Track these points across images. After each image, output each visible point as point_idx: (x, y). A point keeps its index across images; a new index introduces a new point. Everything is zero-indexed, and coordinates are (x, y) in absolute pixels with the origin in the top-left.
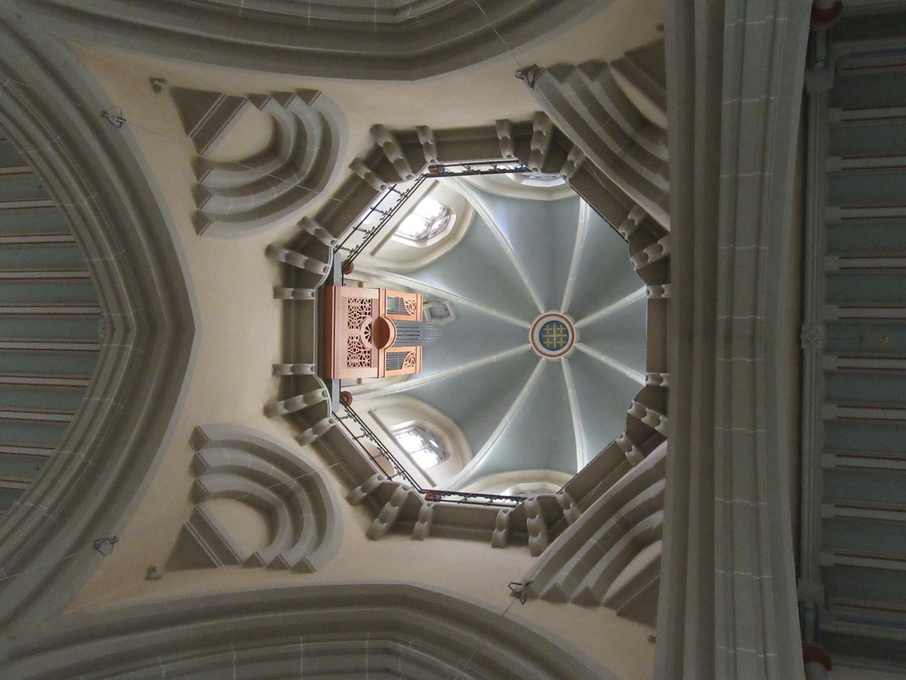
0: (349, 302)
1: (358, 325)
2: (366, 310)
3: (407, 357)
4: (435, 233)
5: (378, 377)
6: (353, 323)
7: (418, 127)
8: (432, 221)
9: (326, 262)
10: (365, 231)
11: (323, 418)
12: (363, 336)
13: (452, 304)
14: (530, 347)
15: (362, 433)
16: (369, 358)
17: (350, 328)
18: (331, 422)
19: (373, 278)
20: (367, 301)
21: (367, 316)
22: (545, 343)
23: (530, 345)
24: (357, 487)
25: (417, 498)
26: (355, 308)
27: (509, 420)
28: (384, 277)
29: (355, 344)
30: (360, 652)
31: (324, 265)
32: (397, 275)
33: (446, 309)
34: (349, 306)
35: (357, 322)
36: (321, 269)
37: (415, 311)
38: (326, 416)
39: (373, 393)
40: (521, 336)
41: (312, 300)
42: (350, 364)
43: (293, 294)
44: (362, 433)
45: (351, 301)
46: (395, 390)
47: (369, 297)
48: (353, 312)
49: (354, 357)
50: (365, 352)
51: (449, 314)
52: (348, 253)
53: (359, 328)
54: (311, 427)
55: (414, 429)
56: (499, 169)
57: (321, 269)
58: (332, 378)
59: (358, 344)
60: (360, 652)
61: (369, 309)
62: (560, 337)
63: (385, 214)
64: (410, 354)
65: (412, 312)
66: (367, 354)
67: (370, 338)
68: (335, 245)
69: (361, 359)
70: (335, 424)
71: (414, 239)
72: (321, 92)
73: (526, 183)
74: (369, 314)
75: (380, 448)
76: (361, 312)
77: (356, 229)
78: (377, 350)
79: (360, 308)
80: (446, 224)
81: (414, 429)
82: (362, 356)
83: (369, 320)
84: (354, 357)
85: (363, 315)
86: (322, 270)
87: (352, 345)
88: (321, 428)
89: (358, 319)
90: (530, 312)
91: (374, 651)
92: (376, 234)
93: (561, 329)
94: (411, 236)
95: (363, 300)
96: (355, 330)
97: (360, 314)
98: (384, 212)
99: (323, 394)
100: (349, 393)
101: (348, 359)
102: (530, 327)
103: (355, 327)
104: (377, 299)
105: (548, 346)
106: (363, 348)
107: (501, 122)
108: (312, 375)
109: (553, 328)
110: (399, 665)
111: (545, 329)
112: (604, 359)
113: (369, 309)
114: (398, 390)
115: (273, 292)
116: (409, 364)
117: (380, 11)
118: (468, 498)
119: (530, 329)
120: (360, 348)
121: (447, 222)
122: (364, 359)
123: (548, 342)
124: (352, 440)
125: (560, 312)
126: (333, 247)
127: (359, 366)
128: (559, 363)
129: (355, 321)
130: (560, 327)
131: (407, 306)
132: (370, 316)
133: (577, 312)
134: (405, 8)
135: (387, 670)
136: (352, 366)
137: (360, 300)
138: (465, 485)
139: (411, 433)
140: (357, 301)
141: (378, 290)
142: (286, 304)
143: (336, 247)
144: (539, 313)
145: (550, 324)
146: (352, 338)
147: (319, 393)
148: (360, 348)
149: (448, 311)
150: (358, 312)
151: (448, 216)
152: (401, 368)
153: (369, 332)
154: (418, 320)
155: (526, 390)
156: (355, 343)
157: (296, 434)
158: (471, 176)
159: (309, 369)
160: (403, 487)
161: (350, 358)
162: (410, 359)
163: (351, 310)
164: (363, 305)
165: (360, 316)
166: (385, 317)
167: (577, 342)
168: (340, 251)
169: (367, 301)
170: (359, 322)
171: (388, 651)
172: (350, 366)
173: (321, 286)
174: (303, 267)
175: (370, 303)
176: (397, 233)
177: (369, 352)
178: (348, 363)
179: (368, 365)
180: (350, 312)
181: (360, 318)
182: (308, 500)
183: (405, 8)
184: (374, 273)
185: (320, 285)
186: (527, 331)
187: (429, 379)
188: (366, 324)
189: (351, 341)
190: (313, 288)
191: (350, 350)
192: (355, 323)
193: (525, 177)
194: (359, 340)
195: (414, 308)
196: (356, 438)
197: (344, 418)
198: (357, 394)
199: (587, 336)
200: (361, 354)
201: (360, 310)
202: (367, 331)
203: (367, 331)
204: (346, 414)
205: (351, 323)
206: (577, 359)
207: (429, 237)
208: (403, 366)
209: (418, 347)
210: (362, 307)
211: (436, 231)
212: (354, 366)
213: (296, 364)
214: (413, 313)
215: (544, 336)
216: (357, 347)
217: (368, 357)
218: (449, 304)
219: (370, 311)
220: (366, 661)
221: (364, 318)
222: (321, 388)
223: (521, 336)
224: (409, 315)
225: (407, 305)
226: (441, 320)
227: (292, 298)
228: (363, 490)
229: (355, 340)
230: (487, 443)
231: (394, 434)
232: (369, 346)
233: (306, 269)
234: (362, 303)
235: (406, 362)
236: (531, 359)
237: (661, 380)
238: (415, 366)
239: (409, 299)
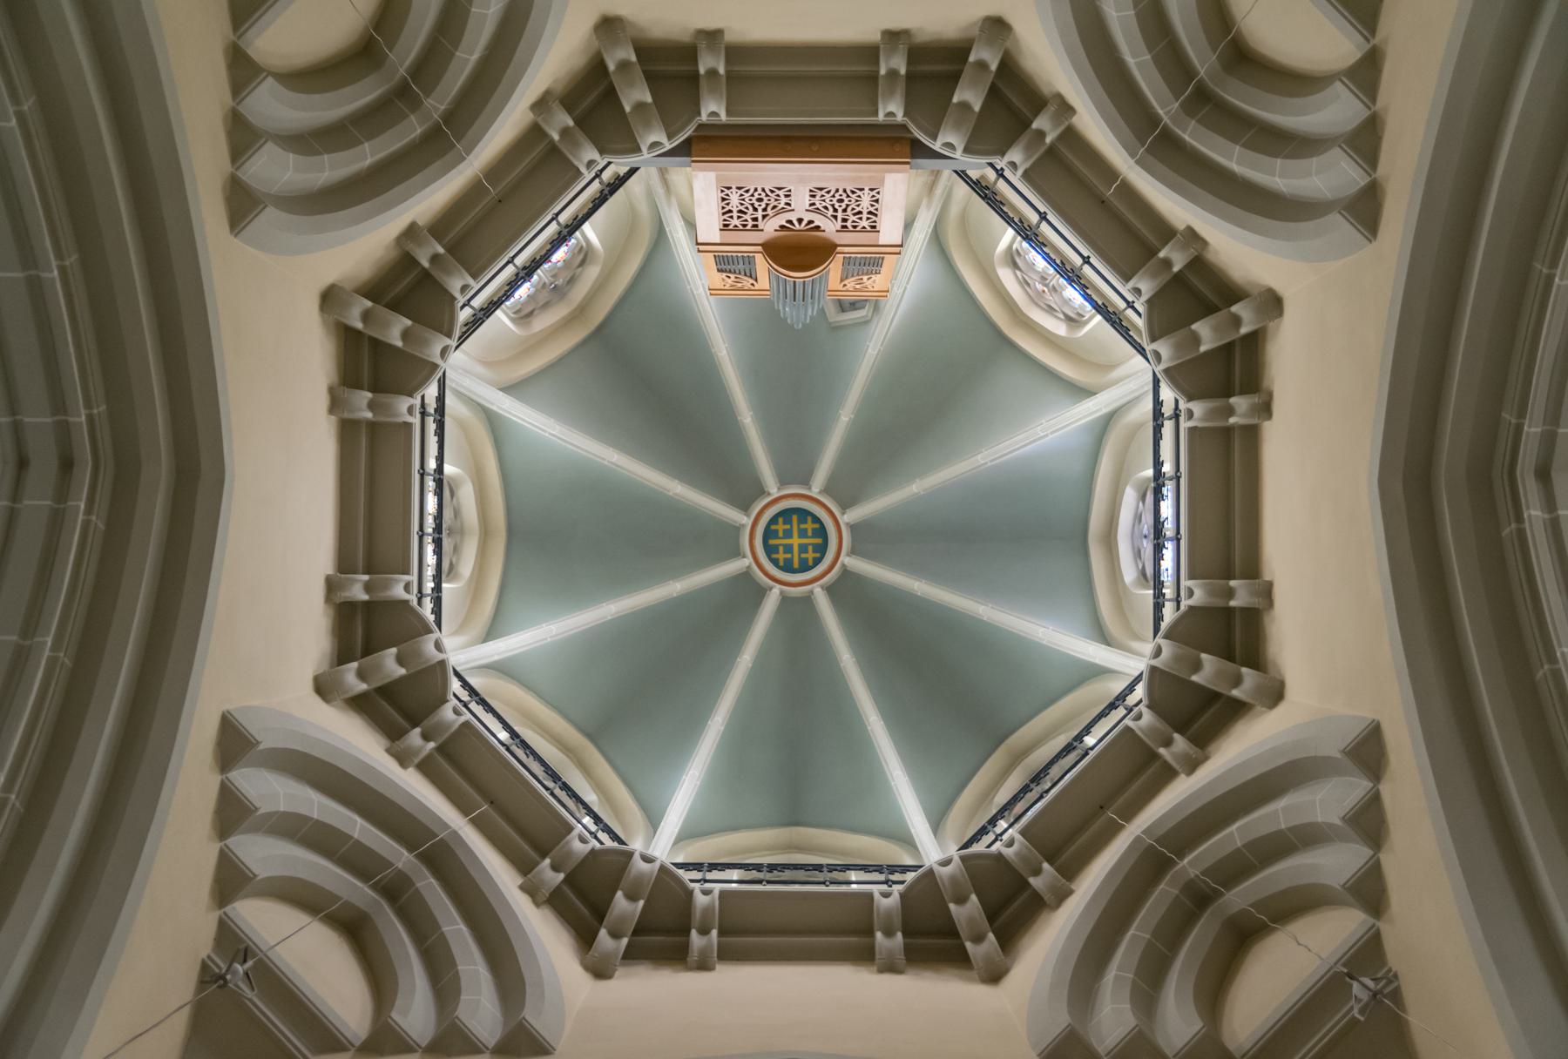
0: (872, 190)
1: (818, 206)
2: (854, 222)
4: (1025, 284)
5: (698, 244)
6: (823, 196)
7: (1270, 395)
12: (794, 217)
14: (771, 491)
16: (741, 227)
17: (811, 191)
20: (875, 222)
21: (839, 223)
23: (774, 492)
24: (440, 243)
25: (424, 382)
26: (857, 201)
28: (929, 206)
29: (773, 200)
30: (59, 404)
35: (824, 204)
36: (952, 139)
40: (795, 469)
41: (876, 113)
45: (874, 193)
49: (743, 200)
50: (755, 219)
51: (843, 310)
53: (812, 208)
54: (575, 123)
55: (582, 247)
56: (1162, 426)
57: (952, 139)
60: (59, 404)
62: (792, 552)
66: (750, 223)
72: (1370, 241)
73: (1129, 497)
74: (843, 227)
78: (760, 242)
79: (858, 209)
80: (1045, 307)
82: (745, 213)
83: (830, 228)
84: (743, 200)
85: (840, 215)
86: (950, 138)
87: (773, 195)
90: (846, 490)
91: (64, 433)
93: (810, 556)
95: (876, 215)
96: (807, 200)
97: (845, 210)
102: (815, 491)
103: (813, 200)
105: (773, 527)
106: (764, 217)
107: (1267, 592)
109: (812, 537)
110: (37, 503)
111: (809, 519)
112: (746, 659)
113: (855, 227)
115: (898, 30)
117: (1549, 441)
118: (432, 418)
120: (765, 210)
123: (781, 527)
125: (848, 555)
127: (723, 208)
128: (737, 553)
130: (814, 552)
132: (839, 228)
133: (847, 591)
134: (1550, 504)
135: (22, 463)
136: (723, 195)
137: (877, 210)
138: (459, 395)
142: (869, 53)
145: (822, 532)
146: (786, 196)
147: (658, 135)
152: (719, 270)
155: (677, 489)
158: (1152, 410)
159: (713, 108)
160: (448, 346)
161: (741, 192)
167: (782, 592)
171: (67, 465)
172: (722, 191)
173: (912, 133)
175: (869, 229)
177: (756, 226)
178: (729, 188)
179: (725, 225)
181: (836, 210)
182: (404, 142)
183: (1550, 504)
185: (913, 131)
186: (806, 482)
187: (697, 289)
188: (819, 220)
189: (781, 193)
190: (904, 116)
192: (824, 201)
193: (1142, 492)
194: (783, 208)
199: (797, 613)
201: (853, 209)
205: (823, 192)
206: (746, 593)
208: (725, 274)
210: (860, 213)
212: (723, 199)
213: (724, 80)
215: (795, 518)
217: (745, 226)
218: (867, 316)
219: (851, 229)
220: (37, 419)
221: (835, 217)
223: (795, 469)
228: (435, 258)
229: (784, 200)
232: (770, 228)
234: (870, 213)
236: (744, 491)
237: (704, 932)
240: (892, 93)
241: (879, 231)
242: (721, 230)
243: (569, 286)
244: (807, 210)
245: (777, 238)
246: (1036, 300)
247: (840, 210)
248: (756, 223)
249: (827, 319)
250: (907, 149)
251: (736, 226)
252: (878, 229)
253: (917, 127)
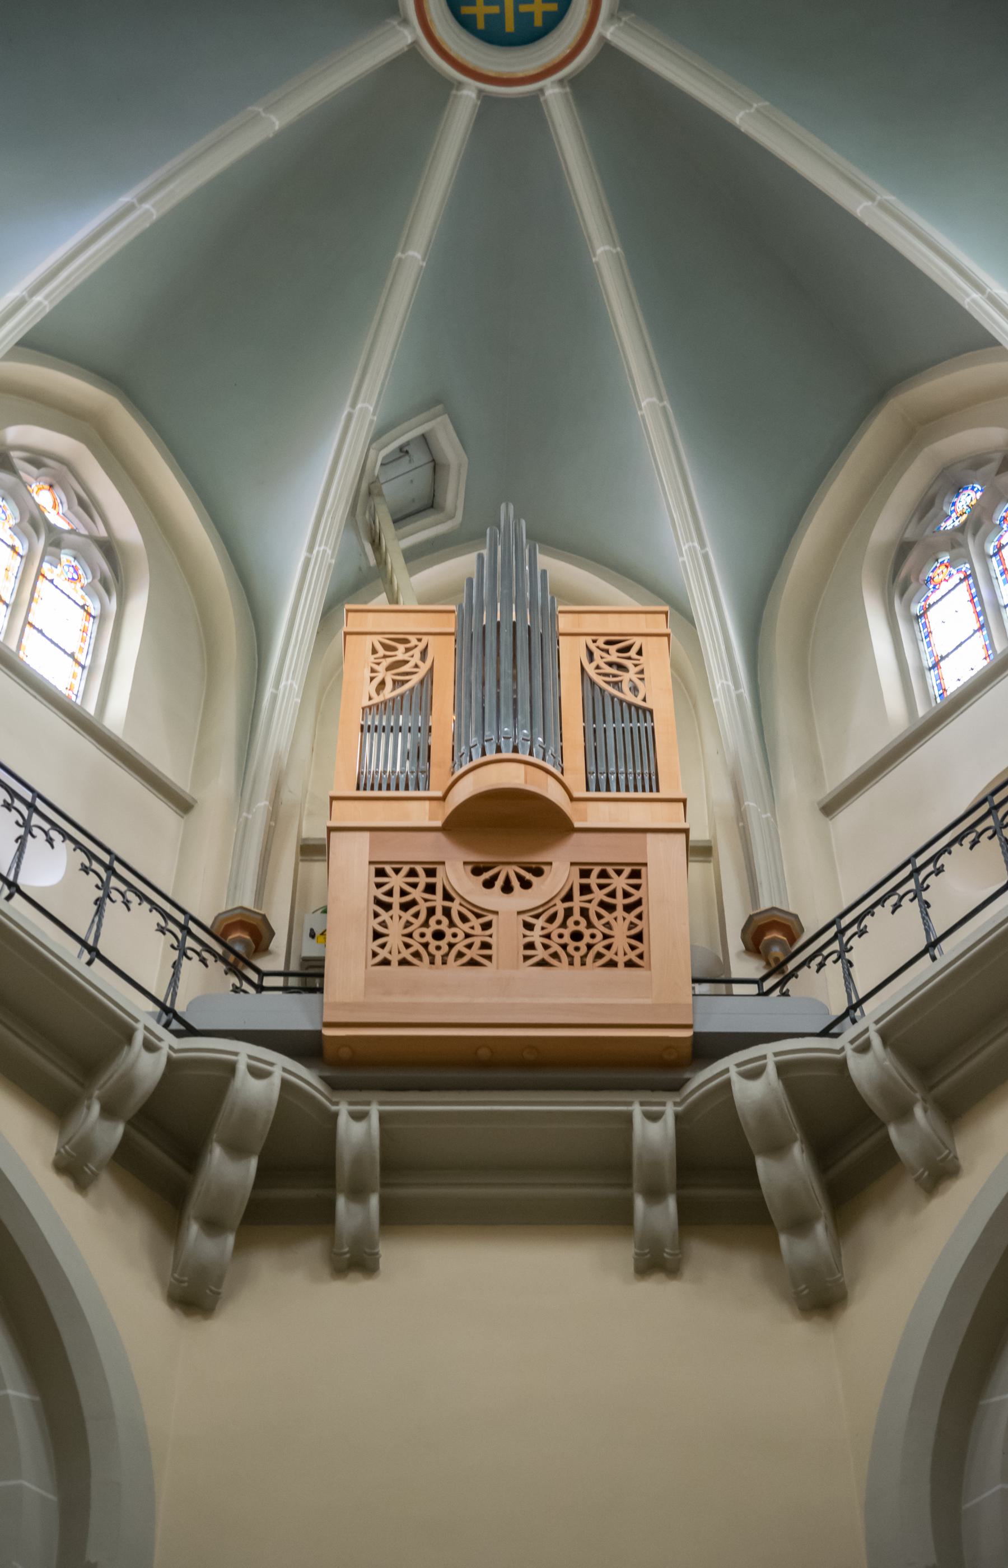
0: (386, 962)
1: (476, 922)
2: (414, 886)
3: (599, 680)
8: (37, 532)
9: (231, 1068)
10: (99, 903)
11: (849, 1077)
12: (522, 900)
13: (379, 434)
14: (557, 90)
15: (910, 909)
16: (610, 870)
17: (489, 958)
18: (864, 1048)
19: (286, 796)
20: (379, 885)
21: (438, 881)
22: (538, 22)
23: (552, 90)
26: (410, 935)
27: (872, 199)
29: (554, 936)
31: (242, 1077)
32: (268, 690)
33: (403, 451)
34: (403, 962)
35: (466, 927)
37: (413, 640)
38: (842, 1065)
39: (750, 803)
41: (383, 1117)
42: (632, 955)
43: (358, 1193)
44: (910, 909)
45: (383, 954)
46: (739, 697)
47: (365, 874)
48: (426, 945)
50: (585, 889)
51: (424, 437)
52: (191, 967)
55: (902, 595)
58: (688, 1033)
59: (551, 919)
61: (412, 873)
63: (26, 825)
64: (590, 669)
65: (416, 659)
66: (593, 881)
67: (529, 870)
68: (159, 1030)
69: (611, 908)
70: (873, 1028)
71: (113, 606)
74: (431, 873)
75: (972, 836)
76: (422, 907)
77: (94, 952)
78: (576, 836)
79: (408, 916)
81: (902, 595)
82: (602, 904)
85: (438, 901)
87: (555, 948)
88: (886, 1089)
89: (452, 924)
92: (108, 852)
94: (102, 618)
95: (378, 902)
97: (431, 911)
98: (21, 831)
99: (754, 1074)
100: (751, 918)
101: (612, 964)
104: (371, 842)
106: (568, 897)
108: (678, 1117)
111: (481, 25)
114: (737, 685)
115: (352, 1275)
116: (633, 670)
119: (480, 91)
120: (569, 912)
121: (37, 459)
122: (612, 894)
124: (942, 961)
126: (168, 1041)
129: (461, 935)
131: (396, 683)
132: (440, 869)
139: (916, 609)
140: (381, 929)
141: (335, 803)
143: (166, 1026)
144: (413, 51)
146: (530, 946)
148: (569, 912)
149: (408, 443)
150: (426, 924)
151: (14, 454)
152: (647, 713)
153: (504, 871)
154: (452, 630)
156: (548, 936)
157: (908, 1188)
161: (609, 955)
162: (610, 664)
163: (417, 955)
164: (396, 900)
165: (439, 914)
166: (443, 798)
168: (180, 1007)
169: (379, 885)
170: (464, 919)
173: (324, 1079)
174: (253, 1163)
175: (388, 869)
176: (91, 708)
177: (585, 874)
178: (630, 964)
179: (636, 874)
180: (426, 958)
181: (447, 912)
184: (262, 804)
189: (540, 953)
190: (335, 1115)
191: (577, 956)
192: (467, 936)
195: (401, 647)
196: (932, 945)
197: (848, 978)
198: (752, 890)
200: (593, 908)
201: (416, 915)
202: (500, 882)
203: (500, 882)
204: (834, 970)
205: (470, 954)
207: (102, 532)
208: (638, 701)
209: (564, 623)
210: (405, 907)
211: (75, 501)
212: (639, 937)
214: (424, 653)
215: (510, 26)
216: (564, 925)
217: (603, 874)
219: (419, 869)
221: (447, 897)
222: (728, 1083)
224: (431, 669)
225: (389, 685)
226: (447, 467)
227: (374, 1201)
229: (536, 936)
230: (966, 303)
231: (921, 711)
233: (259, 1148)
234: (387, 907)
235: (626, 687)
238: (638, 642)
239: (368, 674)
240: (358, 1161)
241: (371, 863)
242: (645, 865)
243: (931, 492)
244: (496, 913)
245: (544, 846)
246: (65, 468)
247: (439, 911)
248: (585, 881)
249: (450, 418)
250: (329, 1050)
251: (619, 873)
252: (373, 868)
253: (313, 1098)
